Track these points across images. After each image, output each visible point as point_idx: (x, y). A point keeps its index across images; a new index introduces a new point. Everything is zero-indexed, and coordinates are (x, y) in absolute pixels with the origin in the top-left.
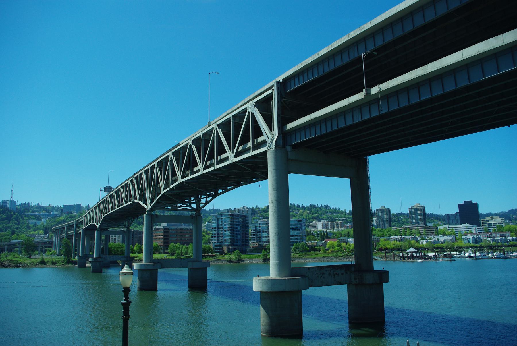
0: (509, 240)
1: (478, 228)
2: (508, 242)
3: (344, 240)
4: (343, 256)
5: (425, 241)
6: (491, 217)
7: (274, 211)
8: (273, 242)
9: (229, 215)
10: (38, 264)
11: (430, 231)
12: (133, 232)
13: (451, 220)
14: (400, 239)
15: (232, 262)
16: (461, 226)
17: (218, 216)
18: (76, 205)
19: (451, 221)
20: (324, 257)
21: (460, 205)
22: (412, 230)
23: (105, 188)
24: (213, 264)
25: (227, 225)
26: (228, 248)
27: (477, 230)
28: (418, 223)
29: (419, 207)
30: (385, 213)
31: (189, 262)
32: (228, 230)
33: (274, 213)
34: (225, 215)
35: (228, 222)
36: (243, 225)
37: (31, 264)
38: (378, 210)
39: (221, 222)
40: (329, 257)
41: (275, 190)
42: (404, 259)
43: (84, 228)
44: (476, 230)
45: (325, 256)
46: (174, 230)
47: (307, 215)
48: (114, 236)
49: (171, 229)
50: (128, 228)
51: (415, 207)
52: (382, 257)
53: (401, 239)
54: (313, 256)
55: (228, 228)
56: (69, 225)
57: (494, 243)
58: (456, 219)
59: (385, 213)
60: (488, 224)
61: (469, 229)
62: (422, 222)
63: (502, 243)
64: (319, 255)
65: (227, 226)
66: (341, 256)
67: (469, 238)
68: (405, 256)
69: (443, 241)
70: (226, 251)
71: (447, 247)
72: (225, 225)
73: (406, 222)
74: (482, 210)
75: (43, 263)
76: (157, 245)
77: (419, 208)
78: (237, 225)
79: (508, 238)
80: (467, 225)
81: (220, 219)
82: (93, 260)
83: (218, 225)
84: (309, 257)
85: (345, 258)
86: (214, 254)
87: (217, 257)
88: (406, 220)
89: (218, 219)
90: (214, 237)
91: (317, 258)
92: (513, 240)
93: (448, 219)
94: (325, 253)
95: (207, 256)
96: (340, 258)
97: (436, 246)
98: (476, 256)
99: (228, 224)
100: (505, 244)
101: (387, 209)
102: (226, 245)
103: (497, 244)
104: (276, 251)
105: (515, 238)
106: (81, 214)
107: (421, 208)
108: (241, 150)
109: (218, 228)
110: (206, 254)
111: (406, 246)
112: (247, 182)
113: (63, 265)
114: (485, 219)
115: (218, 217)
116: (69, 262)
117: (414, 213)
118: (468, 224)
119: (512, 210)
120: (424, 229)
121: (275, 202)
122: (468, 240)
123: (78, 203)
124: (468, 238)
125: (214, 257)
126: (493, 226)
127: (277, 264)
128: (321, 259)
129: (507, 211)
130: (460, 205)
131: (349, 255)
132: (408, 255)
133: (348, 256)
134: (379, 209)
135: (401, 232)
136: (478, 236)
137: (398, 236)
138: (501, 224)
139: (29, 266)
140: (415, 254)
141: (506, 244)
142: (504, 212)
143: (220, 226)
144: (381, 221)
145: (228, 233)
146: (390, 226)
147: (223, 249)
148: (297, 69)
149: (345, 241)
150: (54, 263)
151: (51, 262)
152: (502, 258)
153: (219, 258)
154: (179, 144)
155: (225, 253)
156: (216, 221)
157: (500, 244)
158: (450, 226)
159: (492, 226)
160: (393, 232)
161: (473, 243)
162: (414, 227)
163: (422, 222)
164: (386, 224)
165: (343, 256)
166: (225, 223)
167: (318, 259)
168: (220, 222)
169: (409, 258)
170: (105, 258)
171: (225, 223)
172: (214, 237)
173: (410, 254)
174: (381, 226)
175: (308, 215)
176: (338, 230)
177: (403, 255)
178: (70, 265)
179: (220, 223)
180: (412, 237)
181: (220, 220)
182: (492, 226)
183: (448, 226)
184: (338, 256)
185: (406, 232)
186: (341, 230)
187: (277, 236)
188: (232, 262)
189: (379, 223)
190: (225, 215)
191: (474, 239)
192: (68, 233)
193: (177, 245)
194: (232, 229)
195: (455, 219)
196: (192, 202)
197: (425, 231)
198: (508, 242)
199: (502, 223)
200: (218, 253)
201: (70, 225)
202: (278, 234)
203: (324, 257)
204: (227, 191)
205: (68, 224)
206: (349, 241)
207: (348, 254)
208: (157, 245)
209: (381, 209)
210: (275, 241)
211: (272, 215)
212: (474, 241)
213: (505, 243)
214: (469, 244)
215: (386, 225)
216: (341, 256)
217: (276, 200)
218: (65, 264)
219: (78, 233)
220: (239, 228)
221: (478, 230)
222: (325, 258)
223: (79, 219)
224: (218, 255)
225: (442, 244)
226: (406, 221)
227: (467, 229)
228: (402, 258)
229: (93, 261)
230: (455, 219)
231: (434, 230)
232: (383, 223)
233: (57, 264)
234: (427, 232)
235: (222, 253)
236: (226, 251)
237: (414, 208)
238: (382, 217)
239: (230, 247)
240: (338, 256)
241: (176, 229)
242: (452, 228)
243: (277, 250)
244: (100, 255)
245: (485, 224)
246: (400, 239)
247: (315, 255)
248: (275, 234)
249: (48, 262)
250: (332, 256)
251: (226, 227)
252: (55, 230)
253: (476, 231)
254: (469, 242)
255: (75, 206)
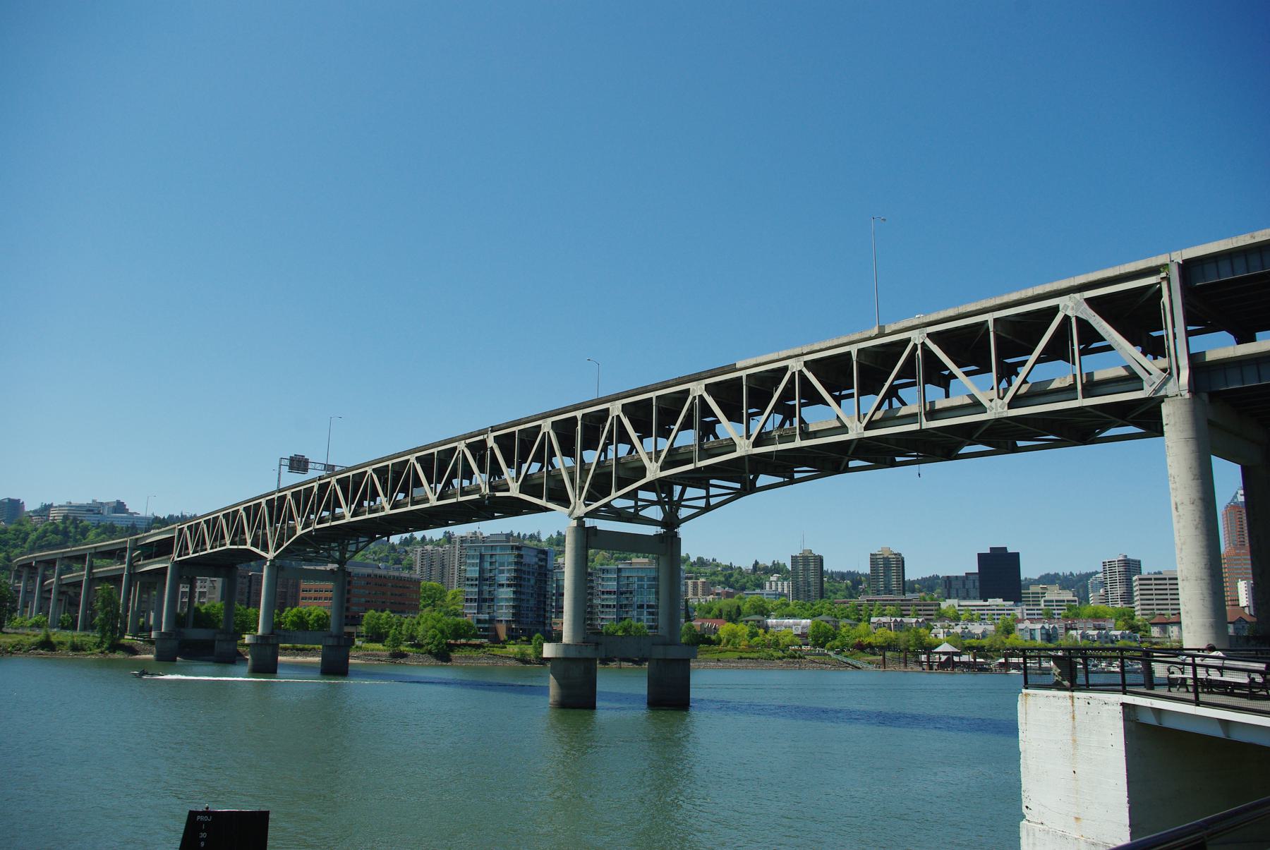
0: (1116, 636)
1: (1027, 610)
2: (1112, 642)
3: (759, 622)
4: (784, 657)
5: (944, 632)
6: (1041, 586)
7: (1197, 519)
8: (1199, 582)
9: (512, 547)
10: (34, 649)
11: (924, 610)
12: (251, 579)
13: (955, 590)
14: (892, 624)
15: (528, 662)
16: (987, 603)
17: (483, 548)
18: (7, 501)
19: (955, 592)
20: (741, 658)
21: (981, 557)
22: (887, 607)
23: (292, 459)
24: (486, 665)
25: (506, 572)
26: (509, 630)
27: (1025, 615)
28: (890, 592)
29: (893, 556)
30: (812, 566)
31: (653, 644)
32: (509, 586)
33: (1199, 523)
34: (503, 548)
35: (509, 564)
36: (539, 574)
37: (15, 648)
38: (796, 557)
39: (491, 563)
40: (753, 659)
41: (1198, 479)
42: (931, 668)
43: (176, 559)
44: (1022, 613)
45: (743, 656)
46: (363, 577)
47: (603, 562)
48: (183, 587)
49: (357, 575)
50: (341, 562)
51: (885, 556)
52: (869, 663)
53: (895, 626)
54: (716, 656)
55: (508, 579)
56: (65, 556)
57: (1085, 641)
58: (966, 587)
59: (812, 566)
60: (1045, 601)
61: (1007, 610)
62: (900, 590)
63: (1101, 643)
64: (729, 655)
65: (506, 575)
66: (779, 658)
67: (1034, 630)
68: (933, 662)
69: (982, 633)
70: (503, 635)
71: (991, 646)
72: (502, 572)
73: (831, 591)
74: (1028, 571)
75: (47, 647)
76: (325, 613)
77: (893, 558)
78: (529, 572)
79: (1113, 633)
80: (999, 601)
81: (489, 556)
82: (257, 640)
83: (482, 571)
84: (705, 656)
85: (789, 663)
86: (477, 641)
87: (489, 650)
88: (832, 586)
89: (482, 557)
90: (471, 600)
91: (727, 660)
92: (1123, 637)
93: (951, 586)
94: (735, 649)
95: (465, 645)
96: (778, 661)
97: (969, 643)
98: (1126, 668)
99: (509, 570)
100: (1107, 646)
101: (816, 556)
102: (502, 621)
103: (1091, 645)
104: (1208, 598)
105: (1127, 632)
106: (23, 525)
107: (898, 558)
108: (1025, 393)
109: (482, 579)
110: (463, 641)
111: (909, 641)
112: (885, 464)
113: (102, 652)
114: (1030, 591)
115: (483, 551)
116: (115, 647)
117: (881, 570)
118: (1002, 600)
119: (1048, 574)
120: (914, 606)
121: (1198, 502)
122: (1031, 634)
123: (12, 497)
124: (1030, 629)
125: (481, 650)
126: (1033, 605)
127: (1212, 625)
128: (733, 662)
129: (1037, 578)
130: (981, 557)
131: (797, 655)
132: (940, 658)
133: (795, 657)
134: (798, 555)
135: (861, 610)
136: (1051, 626)
137: (889, 618)
138: (1073, 604)
139: (13, 653)
140: (956, 659)
141: (1110, 645)
142: (1031, 579)
143: (487, 575)
144: (801, 583)
145: (506, 593)
146: (822, 597)
147: (495, 630)
148: (1235, 245)
149: (761, 623)
150: (76, 648)
151: (68, 644)
152: (1138, 673)
153: (493, 651)
154: (733, 369)
155: (502, 639)
156: (478, 561)
157: (1097, 645)
158: (963, 603)
159: (1053, 605)
160: (842, 610)
161: (1041, 639)
162: (887, 600)
163: (900, 590)
164: (814, 590)
165: (784, 657)
166: (501, 568)
167: (728, 662)
168: (489, 564)
169: (942, 665)
170: (285, 636)
171: (501, 568)
172: (471, 600)
173: (944, 658)
174: (801, 596)
175: (605, 562)
176: (699, 601)
177: (928, 658)
178: (119, 655)
179: (487, 566)
180: (917, 622)
181: (488, 559)
182: (1053, 605)
183: (959, 603)
184: (772, 658)
185: (872, 610)
186: (706, 601)
187: (1209, 569)
188: (528, 662)
189: (798, 589)
190: (503, 548)
191: (1044, 632)
192: (94, 571)
193: (384, 615)
194: (518, 582)
195: (964, 587)
196: (683, 503)
197: (916, 610)
198: (1112, 642)
199: (1075, 601)
200: (486, 640)
201: (101, 552)
202: (1211, 565)
203: (741, 658)
204: (793, 481)
205: (96, 548)
206: (770, 626)
207: (796, 653)
208: (325, 613)
209: (803, 557)
210: (1204, 579)
211: (1194, 528)
212: (1045, 637)
213: (1107, 643)
214: (1033, 642)
215: (812, 594)
216: (779, 658)
217: (1200, 499)
218: (107, 652)
219: (135, 574)
220: (532, 582)
221: (1027, 614)
222: (743, 660)
223: (146, 534)
224: (486, 645)
225: (979, 641)
226: (832, 588)
227: (1004, 610)
228: (925, 667)
229: (257, 643)
230: (964, 587)
231: (932, 610)
232: (806, 589)
233: (85, 651)
234: (920, 612)
235: (495, 640)
236: (503, 635)
237: (883, 558)
238: (804, 575)
239: (514, 626)
240: (772, 658)
241: (369, 575)
242: (966, 608)
243: (1210, 597)
244: (273, 629)
245: (1039, 601)
246: (892, 624)
247: (720, 652)
248: (1203, 567)
249: (62, 643)
250: (759, 658)
251: (503, 578)
252: (37, 562)
253: (1023, 616)
254: (1033, 638)
255: (4, 503)
